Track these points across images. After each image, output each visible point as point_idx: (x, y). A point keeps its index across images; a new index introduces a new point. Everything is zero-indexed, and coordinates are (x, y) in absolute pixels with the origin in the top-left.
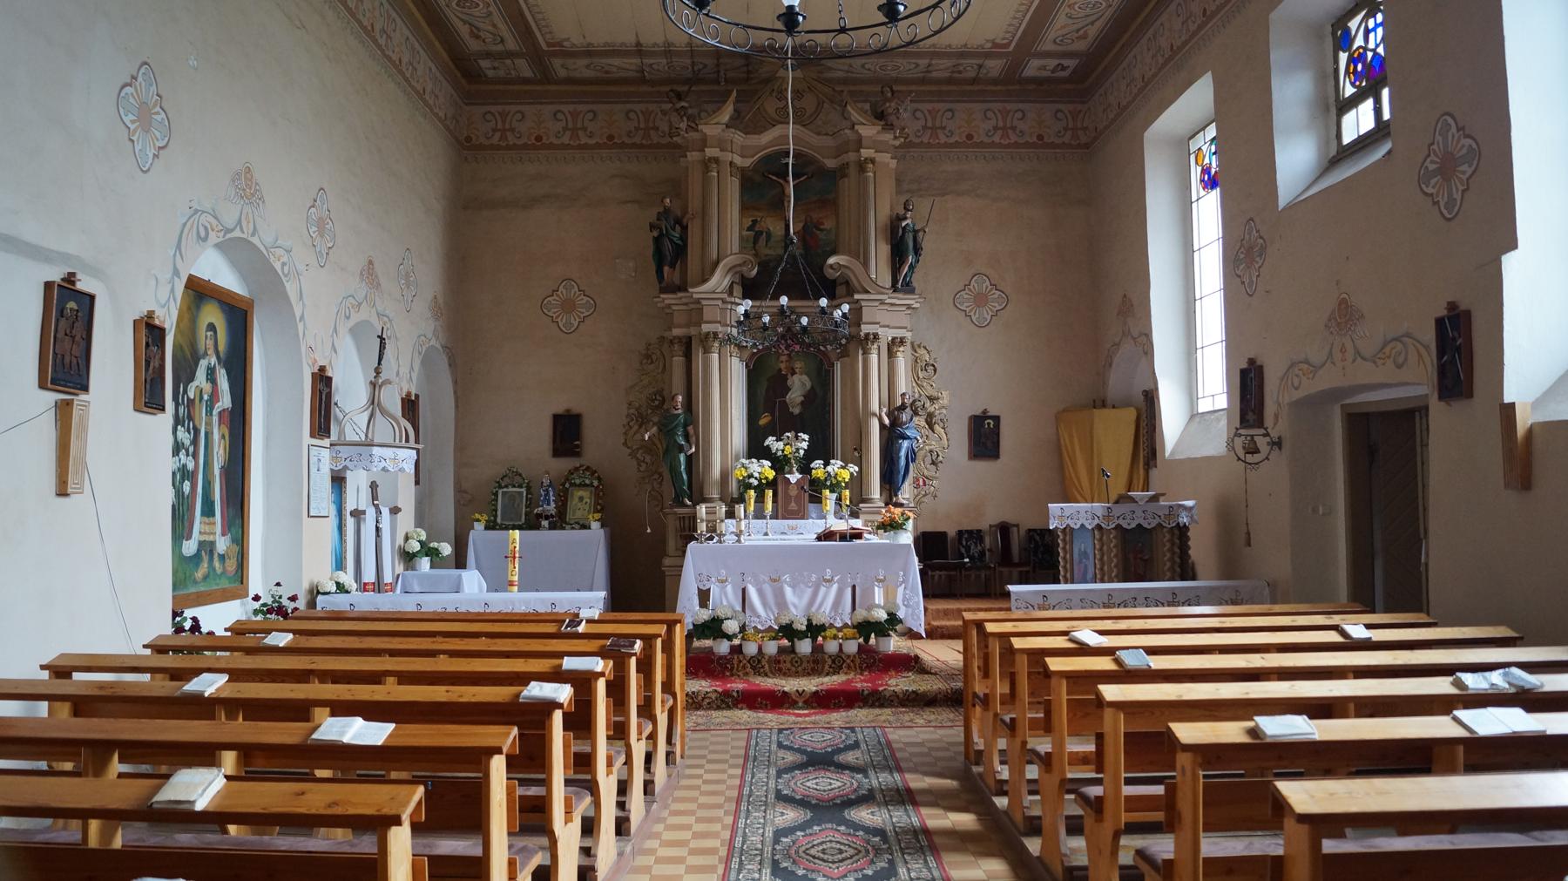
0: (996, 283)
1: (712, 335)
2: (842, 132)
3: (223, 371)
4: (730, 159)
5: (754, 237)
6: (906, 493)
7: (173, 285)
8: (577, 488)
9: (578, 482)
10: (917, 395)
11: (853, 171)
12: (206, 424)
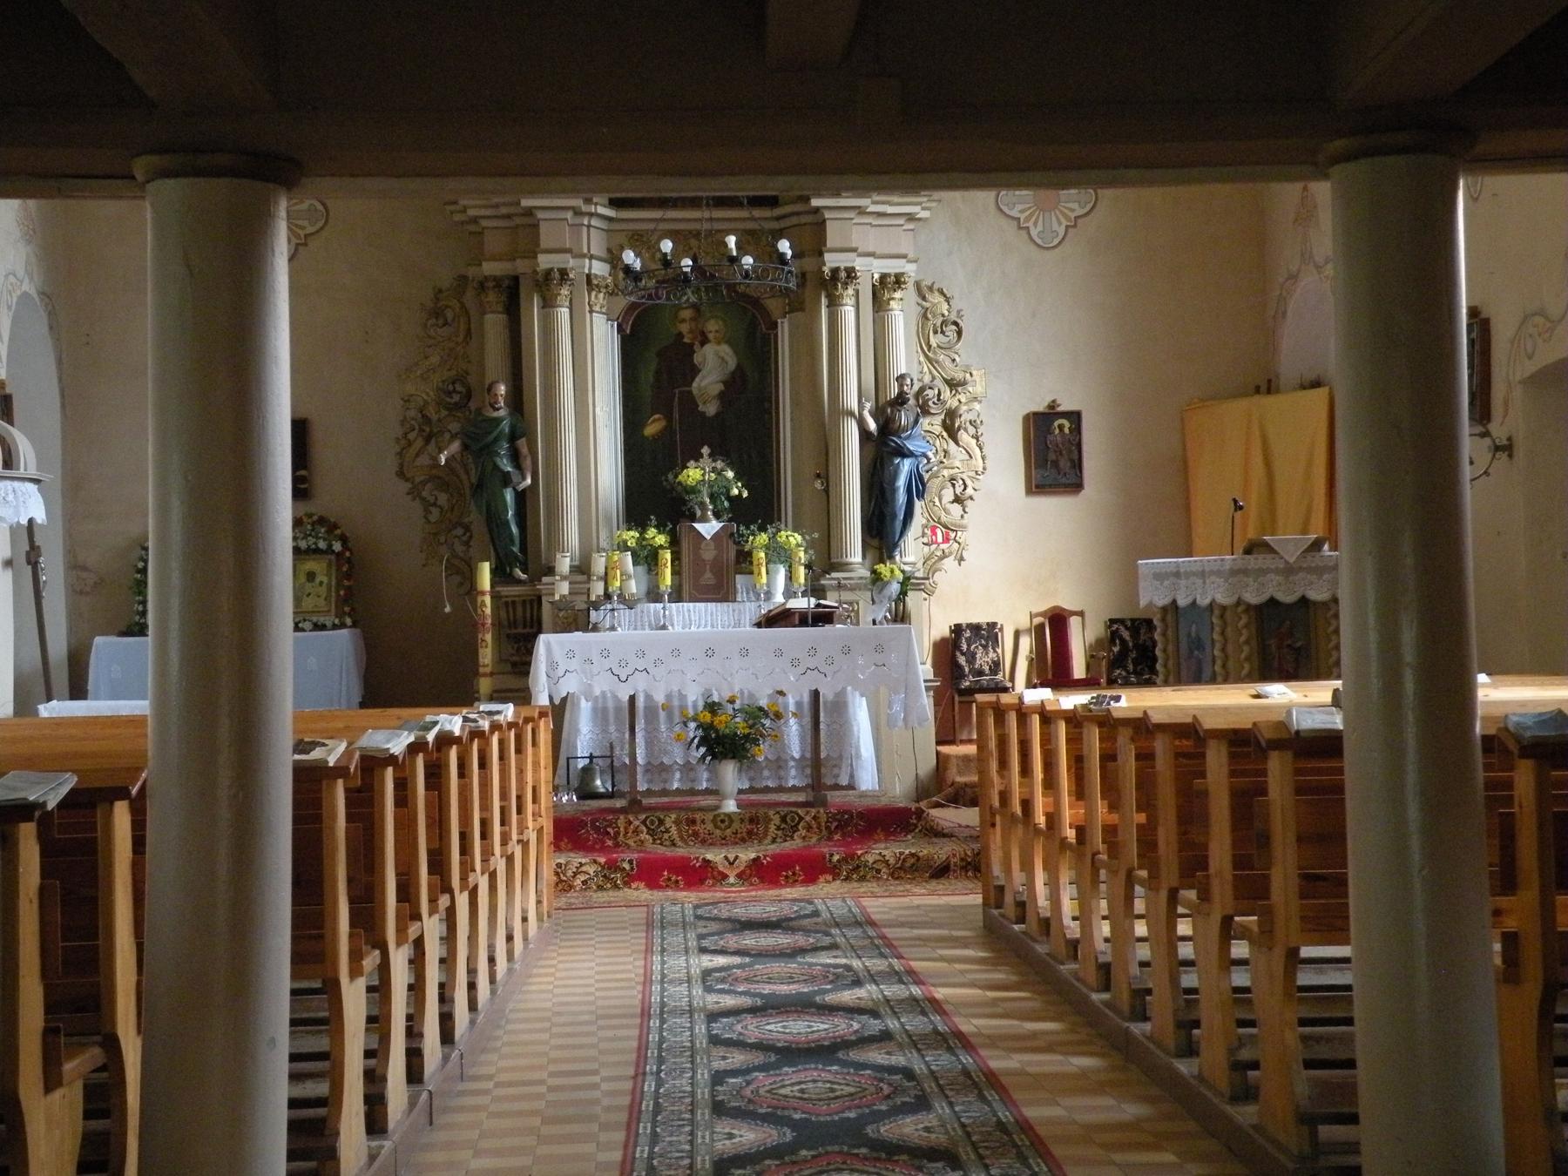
1: (557, 275)
10: (927, 379)
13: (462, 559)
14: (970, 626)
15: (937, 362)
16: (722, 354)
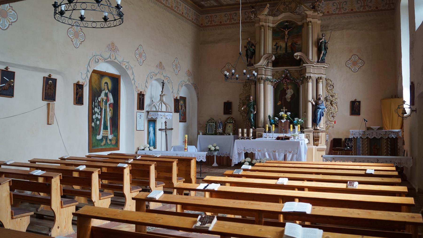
0: (360, 57)
1: (261, 78)
2: (302, 14)
3: (110, 94)
4: (268, 25)
5: (276, 47)
6: (322, 125)
7: (87, 74)
8: (229, 123)
9: (229, 121)
10: (327, 95)
11: (305, 25)
12: (105, 107)
13: (248, 125)
14: (348, 138)
15: (329, 92)
16: (291, 91)
